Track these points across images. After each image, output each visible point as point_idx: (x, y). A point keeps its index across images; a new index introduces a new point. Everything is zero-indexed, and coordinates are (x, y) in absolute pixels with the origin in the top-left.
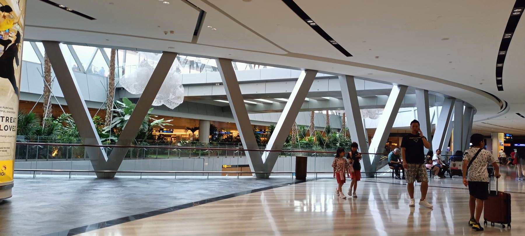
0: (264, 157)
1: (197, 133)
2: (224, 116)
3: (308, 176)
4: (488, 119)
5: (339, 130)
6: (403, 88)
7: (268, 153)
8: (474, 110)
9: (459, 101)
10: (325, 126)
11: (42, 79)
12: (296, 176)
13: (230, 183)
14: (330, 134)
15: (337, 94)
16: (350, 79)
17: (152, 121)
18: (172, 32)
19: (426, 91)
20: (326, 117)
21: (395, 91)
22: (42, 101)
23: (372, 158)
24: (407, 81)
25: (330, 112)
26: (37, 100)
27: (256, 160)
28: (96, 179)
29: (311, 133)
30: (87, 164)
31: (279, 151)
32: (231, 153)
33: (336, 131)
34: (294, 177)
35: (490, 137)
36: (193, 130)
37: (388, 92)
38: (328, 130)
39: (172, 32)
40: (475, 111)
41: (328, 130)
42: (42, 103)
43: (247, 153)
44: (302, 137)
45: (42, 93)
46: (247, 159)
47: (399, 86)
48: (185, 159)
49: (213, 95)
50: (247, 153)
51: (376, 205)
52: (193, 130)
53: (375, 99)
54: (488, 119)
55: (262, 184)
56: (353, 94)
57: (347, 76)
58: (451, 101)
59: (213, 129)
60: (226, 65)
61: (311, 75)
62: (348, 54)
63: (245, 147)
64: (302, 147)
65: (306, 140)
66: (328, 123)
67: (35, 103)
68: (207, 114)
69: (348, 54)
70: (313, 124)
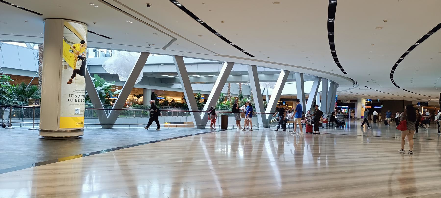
0: (202, 115)
1: (141, 99)
2: (162, 86)
3: (229, 127)
4: (349, 89)
5: (248, 96)
6: (287, 73)
7: (204, 113)
8: (336, 86)
9: (324, 79)
10: (238, 93)
11: (37, 61)
12: (222, 127)
13: (185, 131)
14: (242, 100)
15: (247, 73)
16: (254, 67)
17: (115, 91)
18: (153, 45)
19: (302, 74)
20: (239, 87)
21: (283, 74)
22: (37, 76)
23: (267, 116)
24: (288, 69)
25: (242, 83)
26: (34, 76)
27: (197, 118)
28: (101, 129)
29: (228, 99)
30: (97, 121)
31: (212, 111)
32: (181, 114)
33: (246, 97)
34: (220, 128)
35: (356, 101)
36: (138, 97)
37: (279, 73)
38: (241, 97)
39: (153, 45)
40: (337, 86)
41: (241, 97)
42: (38, 78)
43: (191, 113)
44: (221, 102)
45: (38, 71)
46: (191, 119)
47: (285, 71)
48: (139, 118)
49: (159, 72)
50: (191, 113)
51: (269, 145)
52: (138, 97)
53: (272, 76)
54: (349, 89)
55: (201, 131)
56: (256, 74)
57: (252, 65)
58: (319, 79)
59: (154, 96)
60: (179, 59)
61: (231, 65)
62: (252, 56)
63: (190, 109)
64: (221, 110)
65: (224, 104)
66: (240, 91)
67: (32, 78)
68: (150, 84)
69: (252, 56)
70: (229, 92)
